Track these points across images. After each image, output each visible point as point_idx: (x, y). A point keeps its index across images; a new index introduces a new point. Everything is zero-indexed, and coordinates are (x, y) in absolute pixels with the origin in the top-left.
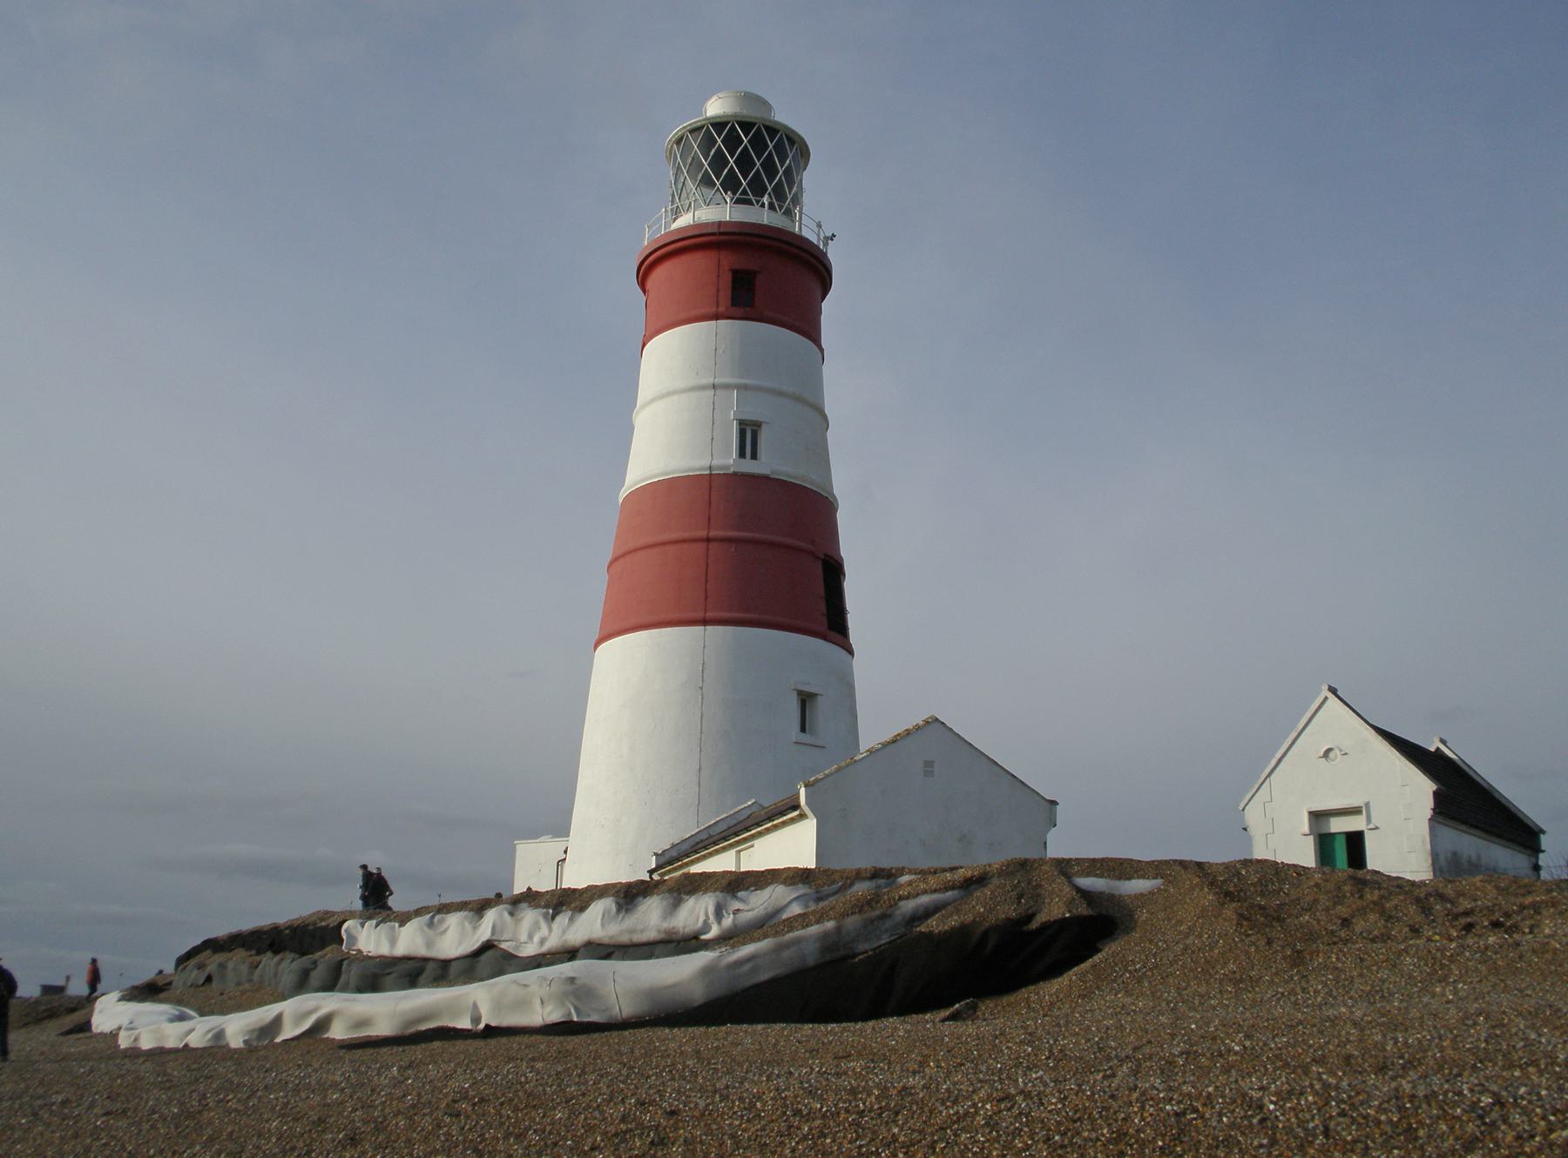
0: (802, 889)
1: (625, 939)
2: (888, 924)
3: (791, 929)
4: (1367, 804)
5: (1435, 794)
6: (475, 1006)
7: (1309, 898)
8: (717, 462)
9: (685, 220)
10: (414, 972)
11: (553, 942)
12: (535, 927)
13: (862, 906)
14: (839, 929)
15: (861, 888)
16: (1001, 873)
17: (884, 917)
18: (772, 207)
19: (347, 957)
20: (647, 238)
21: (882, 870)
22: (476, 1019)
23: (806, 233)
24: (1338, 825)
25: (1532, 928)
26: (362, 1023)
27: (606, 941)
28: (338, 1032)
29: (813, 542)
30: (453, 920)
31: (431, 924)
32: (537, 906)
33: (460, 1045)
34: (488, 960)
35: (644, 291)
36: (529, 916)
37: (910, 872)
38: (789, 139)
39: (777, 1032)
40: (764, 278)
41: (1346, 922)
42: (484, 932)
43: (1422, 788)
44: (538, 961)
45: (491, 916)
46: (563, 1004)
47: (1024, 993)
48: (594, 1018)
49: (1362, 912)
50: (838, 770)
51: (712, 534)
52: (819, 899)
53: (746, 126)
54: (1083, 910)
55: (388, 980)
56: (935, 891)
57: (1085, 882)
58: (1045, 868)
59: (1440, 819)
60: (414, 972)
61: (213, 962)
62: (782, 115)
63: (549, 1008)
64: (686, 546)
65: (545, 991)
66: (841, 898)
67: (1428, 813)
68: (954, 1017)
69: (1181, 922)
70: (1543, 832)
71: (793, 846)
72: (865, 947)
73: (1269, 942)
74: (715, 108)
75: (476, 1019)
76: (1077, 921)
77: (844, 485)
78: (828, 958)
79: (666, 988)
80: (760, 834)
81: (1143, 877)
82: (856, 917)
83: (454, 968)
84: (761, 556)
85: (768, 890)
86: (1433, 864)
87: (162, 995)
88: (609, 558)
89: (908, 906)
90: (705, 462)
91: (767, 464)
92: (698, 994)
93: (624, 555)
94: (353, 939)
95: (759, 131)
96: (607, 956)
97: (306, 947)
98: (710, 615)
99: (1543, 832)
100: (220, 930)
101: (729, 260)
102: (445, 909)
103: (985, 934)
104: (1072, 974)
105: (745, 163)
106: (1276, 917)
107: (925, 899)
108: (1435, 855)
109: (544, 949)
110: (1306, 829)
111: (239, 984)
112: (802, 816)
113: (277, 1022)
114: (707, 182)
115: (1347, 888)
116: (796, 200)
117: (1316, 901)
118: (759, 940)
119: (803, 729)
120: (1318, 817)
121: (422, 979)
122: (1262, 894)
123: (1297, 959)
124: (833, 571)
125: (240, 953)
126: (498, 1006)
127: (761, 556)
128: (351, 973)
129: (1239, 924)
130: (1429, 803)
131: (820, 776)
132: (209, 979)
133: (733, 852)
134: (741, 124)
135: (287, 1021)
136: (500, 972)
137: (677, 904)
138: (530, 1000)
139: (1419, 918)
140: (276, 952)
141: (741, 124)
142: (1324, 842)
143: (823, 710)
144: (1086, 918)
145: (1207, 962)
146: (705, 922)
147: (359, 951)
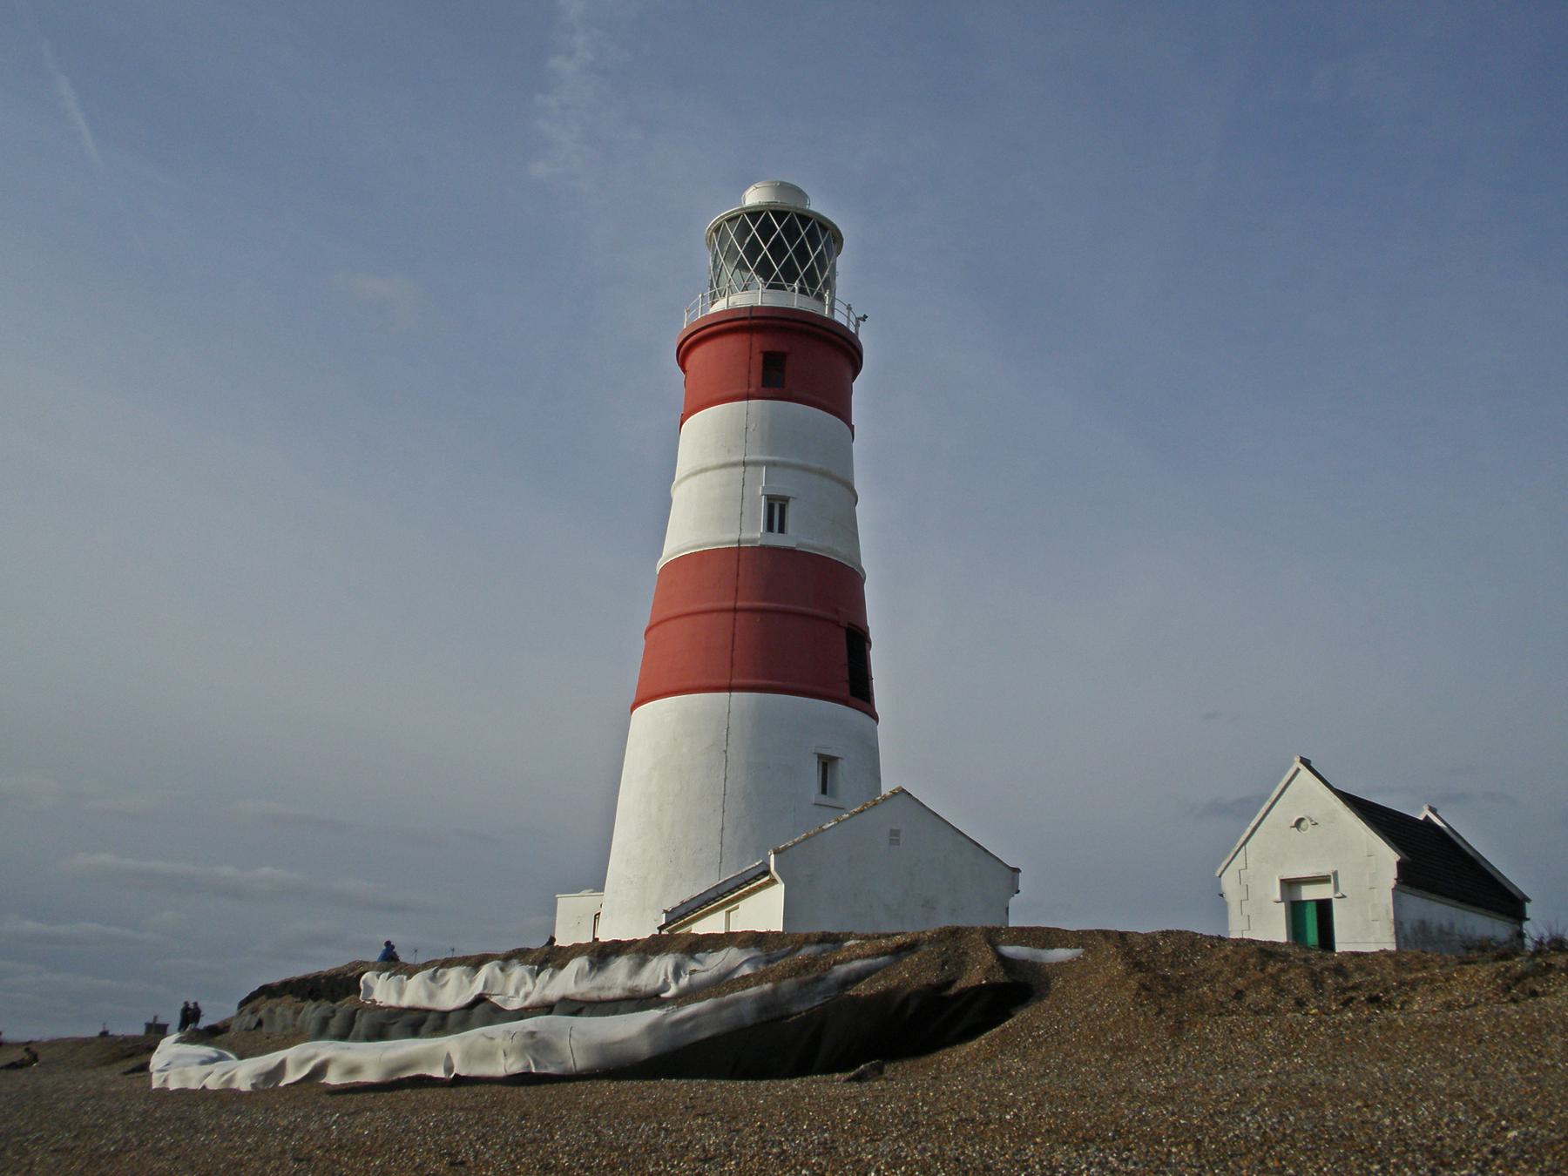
0: (753, 952)
1: (594, 995)
2: (821, 986)
3: (732, 991)
4: (1335, 874)
5: (1399, 864)
6: (449, 1057)
7: (1213, 971)
8: (746, 535)
9: (720, 305)
10: (418, 1022)
11: (534, 998)
12: (522, 983)
13: (796, 971)
14: (774, 991)
15: (808, 951)
16: (931, 941)
17: (818, 979)
18: (802, 291)
19: (362, 1007)
20: (687, 321)
21: (830, 934)
22: (449, 1069)
23: (839, 318)
24: (1309, 893)
25: (1403, 1003)
26: (353, 1070)
27: (578, 997)
28: (333, 1078)
29: (837, 612)
30: (453, 974)
31: (433, 978)
32: (525, 963)
33: (427, 1093)
34: (481, 1010)
35: (684, 371)
36: (518, 971)
37: (856, 938)
38: (821, 225)
39: (718, 1088)
40: (795, 359)
41: (1239, 995)
42: (478, 988)
43: (1387, 858)
44: (521, 1014)
45: (485, 970)
46: (523, 1056)
47: (939, 1055)
48: (551, 1070)
49: (1257, 985)
50: (806, 838)
51: (740, 604)
52: (769, 962)
53: (780, 215)
54: (1000, 977)
55: (394, 1029)
56: (868, 956)
57: (1009, 950)
58: (975, 936)
59: (1407, 888)
60: (418, 1022)
61: (265, 1006)
62: (816, 206)
63: (511, 1060)
64: (699, 618)
65: (507, 1044)
66: (788, 960)
67: (1392, 883)
68: (859, 1078)
69: (1089, 991)
70: (1529, 900)
71: (764, 911)
72: (800, 1008)
73: (1161, 1011)
74: (754, 197)
75: (449, 1069)
76: (993, 988)
77: (869, 563)
78: (764, 1018)
79: (622, 1041)
80: (743, 896)
81: (1066, 946)
82: (792, 980)
83: (452, 1019)
84: (789, 626)
85: (724, 952)
86: (1397, 933)
87: (219, 1038)
88: (646, 623)
89: (841, 970)
90: (735, 536)
91: (793, 537)
92: (644, 1049)
93: (658, 624)
94: (369, 990)
95: (792, 218)
96: (577, 1013)
97: (329, 998)
98: (735, 681)
99: (1529, 900)
100: (275, 978)
101: (760, 343)
102: (448, 963)
103: (906, 1000)
104: (983, 1039)
105: (778, 249)
106: (1176, 988)
107: (857, 964)
108: (1398, 924)
109: (527, 1003)
110: (1278, 896)
111: (285, 1028)
112: (773, 882)
113: (281, 1068)
114: (741, 266)
115: (1252, 960)
116: (828, 284)
117: (1220, 972)
118: (703, 1000)
119: (824, 791)
120: (1289, 885)
121: (424, 1029)
122: (1172, 966)
123: (1178, 1029)
124: (858, 640)
125: (289, 999)
126: (468, 1056)
127: (789, 626)
128: (362, 1023)
129: (1138, 995)
130: (1392, 873)
131: (789, 844)
132: (260, 1023)
133: (723, 913)
134: (775, 213)
135: (290, 1067)
136: (489, 1022)
137: (642, 964)
138: (493, 1053)
139: (1309, 992)
140: (315, 1000)
141: (775, 213)
142: (1296, 910)
143: (843, 773)
144: (1005, 985)
145: (1102, 1029)
146: (665, 981)
147: (374, 1001)
